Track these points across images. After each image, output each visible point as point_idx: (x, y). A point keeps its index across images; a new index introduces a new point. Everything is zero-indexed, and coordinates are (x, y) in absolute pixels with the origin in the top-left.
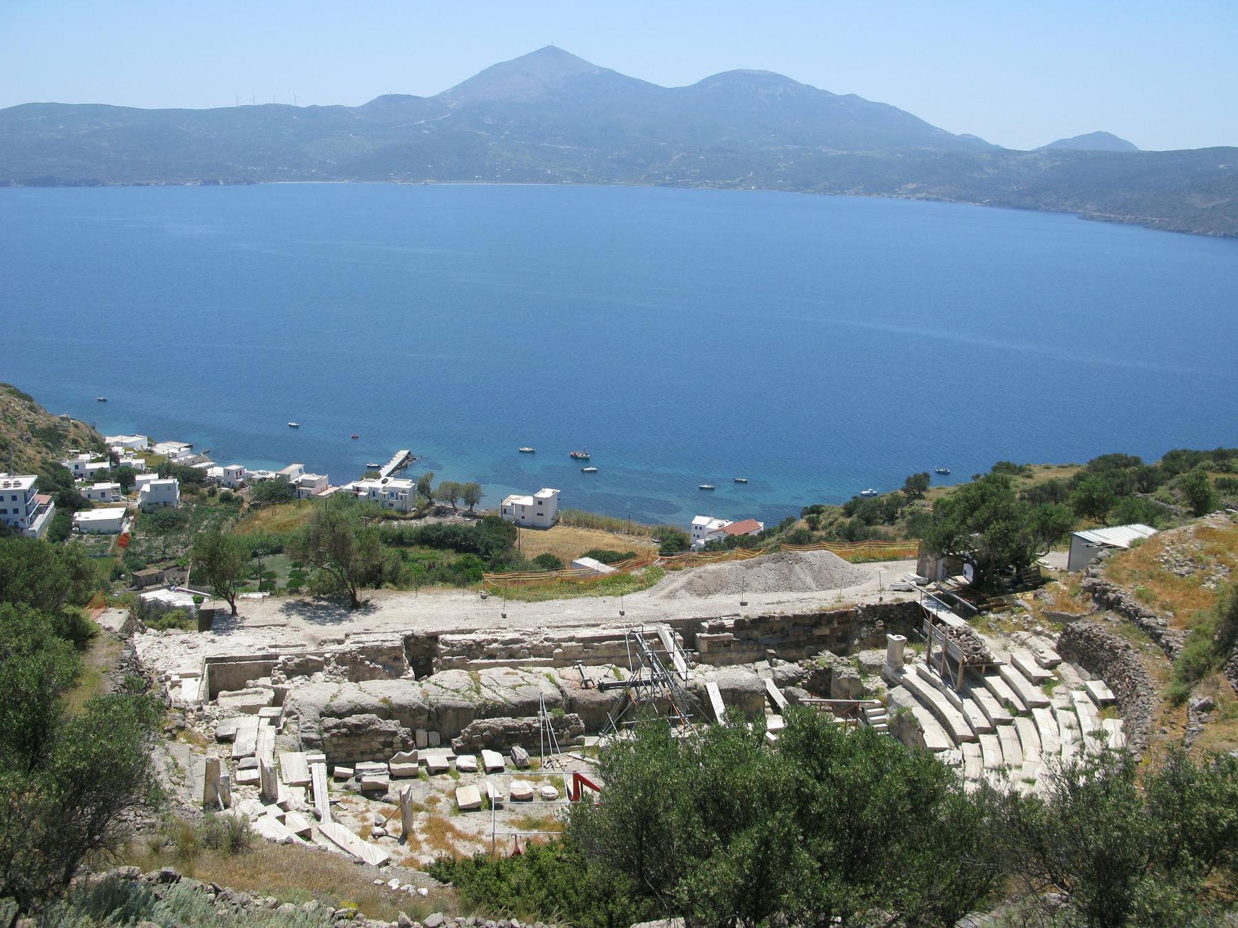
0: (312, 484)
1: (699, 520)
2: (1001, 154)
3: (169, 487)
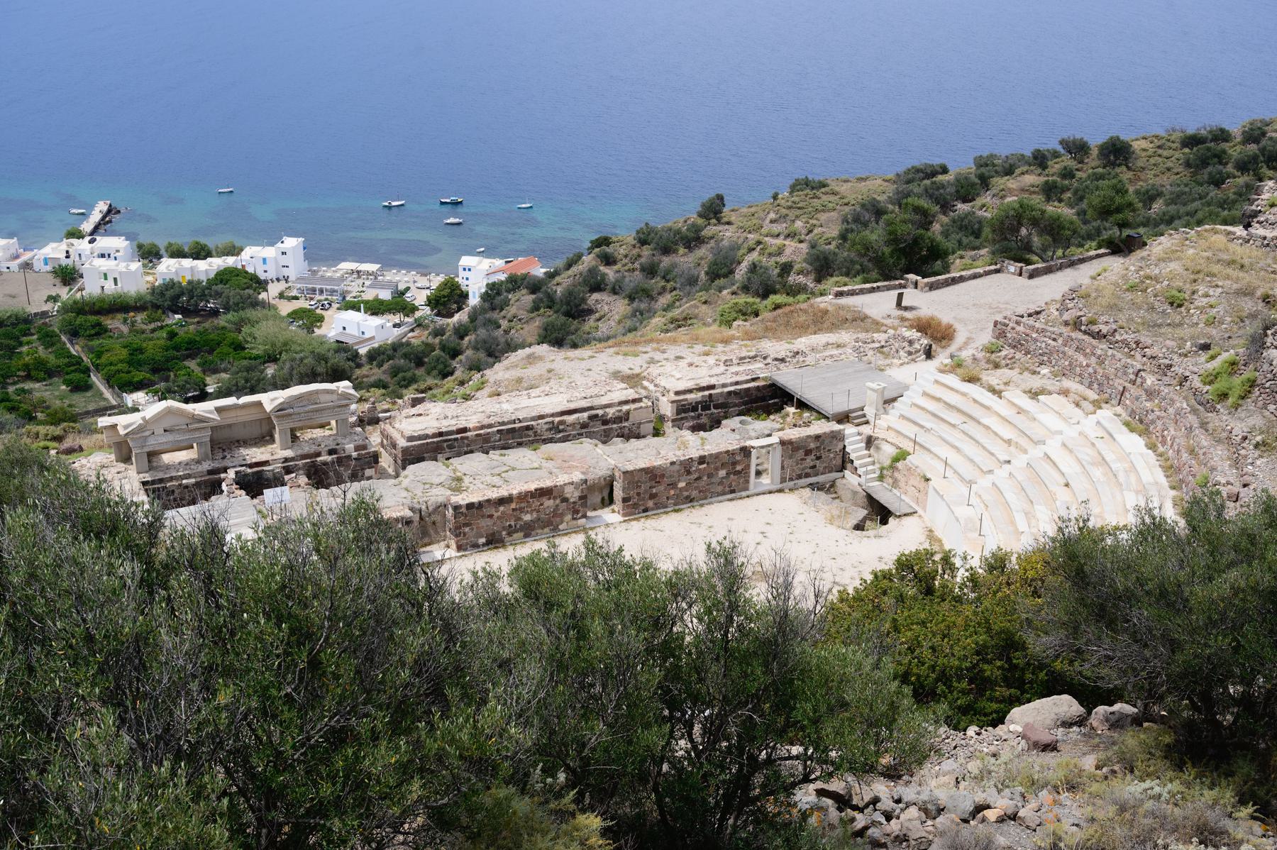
1: (466, 261)
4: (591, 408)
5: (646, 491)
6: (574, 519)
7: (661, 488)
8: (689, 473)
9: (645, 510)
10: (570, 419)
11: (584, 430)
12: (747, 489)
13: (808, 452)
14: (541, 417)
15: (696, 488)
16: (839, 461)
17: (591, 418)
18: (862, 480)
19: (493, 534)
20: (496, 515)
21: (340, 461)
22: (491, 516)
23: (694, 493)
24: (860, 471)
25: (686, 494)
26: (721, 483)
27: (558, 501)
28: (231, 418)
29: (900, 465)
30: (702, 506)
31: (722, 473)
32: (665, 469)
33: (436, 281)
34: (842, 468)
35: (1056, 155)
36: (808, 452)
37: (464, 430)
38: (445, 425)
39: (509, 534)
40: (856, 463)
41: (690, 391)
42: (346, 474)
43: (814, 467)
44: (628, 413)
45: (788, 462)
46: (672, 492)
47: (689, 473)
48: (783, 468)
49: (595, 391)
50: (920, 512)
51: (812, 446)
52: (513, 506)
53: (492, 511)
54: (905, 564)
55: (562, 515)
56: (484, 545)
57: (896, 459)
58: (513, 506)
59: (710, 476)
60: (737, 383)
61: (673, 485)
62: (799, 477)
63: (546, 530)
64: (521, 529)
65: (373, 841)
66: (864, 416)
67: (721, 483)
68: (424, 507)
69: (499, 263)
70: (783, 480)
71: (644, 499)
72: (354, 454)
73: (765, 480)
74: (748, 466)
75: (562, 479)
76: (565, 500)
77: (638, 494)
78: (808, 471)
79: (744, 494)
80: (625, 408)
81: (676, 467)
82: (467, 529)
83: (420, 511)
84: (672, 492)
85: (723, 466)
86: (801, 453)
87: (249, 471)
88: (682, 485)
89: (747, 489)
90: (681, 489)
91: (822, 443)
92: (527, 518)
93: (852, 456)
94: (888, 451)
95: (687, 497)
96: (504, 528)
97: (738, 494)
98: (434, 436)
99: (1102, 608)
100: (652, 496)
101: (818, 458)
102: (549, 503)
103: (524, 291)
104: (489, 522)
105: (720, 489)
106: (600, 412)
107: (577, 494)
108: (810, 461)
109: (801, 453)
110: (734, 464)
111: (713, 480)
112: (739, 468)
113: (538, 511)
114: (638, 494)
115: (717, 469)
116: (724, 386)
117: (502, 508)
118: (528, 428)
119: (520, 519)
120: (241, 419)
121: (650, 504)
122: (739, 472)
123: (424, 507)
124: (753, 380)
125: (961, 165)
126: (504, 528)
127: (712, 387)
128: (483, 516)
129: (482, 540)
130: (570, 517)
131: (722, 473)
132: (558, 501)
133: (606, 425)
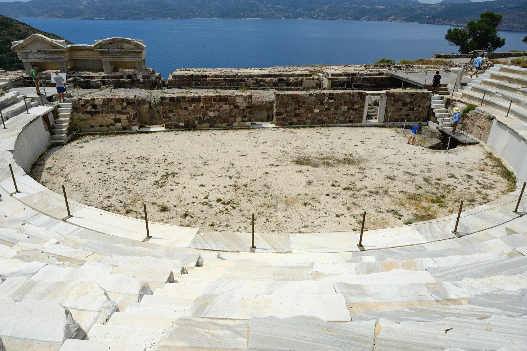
4: (281, 76)
5: (291, 111)
6: (243, 121)
7: (303, 110)
8: (322, 104)
9: (292, 124)
10: (267, 79)
12: (361, 122)
13: (405, 104)
15: (326, 115)
16: (425, 114)
18: (440, 126)
19: (189, 121)
20: (190, 108)
22: (186, 109)
23: (325, 119)
24: (439, 120)
25: (319, 118)
26: (343, 115)
27: (232, 107)
29: (469, 114)
30: (329, 126)
31: (345, 108)
32: (305, 98)
34: (427, 119)
36: (405, 104)
39: (200, 123)
40: (437, 115)
41: (341, 75)
43: (408, 115)
44: (302, 81)
45: (390, 109)
46: (310, 115)
47: (322, 104)
48: (386, 112)
50: (482, 143)
51: (408, 100)
52: (201, 104)
53: (187, 105)
54: (404, 268)
55: (235, 117)
56: (183, 127)
57: (467, 111)
58: (201, 104)
59: (336, 108)
60: (370, 75)
61: (311, 110)
62: (397, 120)
63: (225, 125)
64: (208, 121)
66: (446, 89)
67: (343, 115)
68: (153, 101)
70: (385, 120)
71: (290, 116)
72: (141, 80)
73: (374, 121)
74: (363, 107)
76: (237, 107)
77: (287, 112)
78: (404, 117)
79: (358, 124)
80: (300, 78)
81: (313, 98)
82: (171, 115)
83: (150, 103)
84: (310, 115)
85: (346, 103)
86: (400, 104)
87: (82, 80)
88: (317, 111)
89: (361, 122)
90: (316, 114)
91: (415, 100)
92: (211, 114)
93: (435, 110)
94: (459, 108)
95: (320, 120)
96: (196, 119)
97: (354, 124)
100: (296, 115)
101: (412, 110)
102: (226, 107)
104: (185, 113)
105: (342, 118)
106: (285, 78)
107: (245, 104)
108: (405, 111)
109: (400, 104)
110: (354, 103)
111: (338, 112)
112: (356, 106)
113: (219, 111)
114: (287, 112)
115: (341, 105)
116: (362, 75)
117: (193, 105)
119: (206, 114)
120: (91, 57)
121: (295, 120)
122: (356, 110)
123: (153, 101)
124: (380, 74)
126: (196, 119)
128: (181, 108)
129: (182, 124)
130: (239, 119)
131: (345, 108)
132: (232, 107)
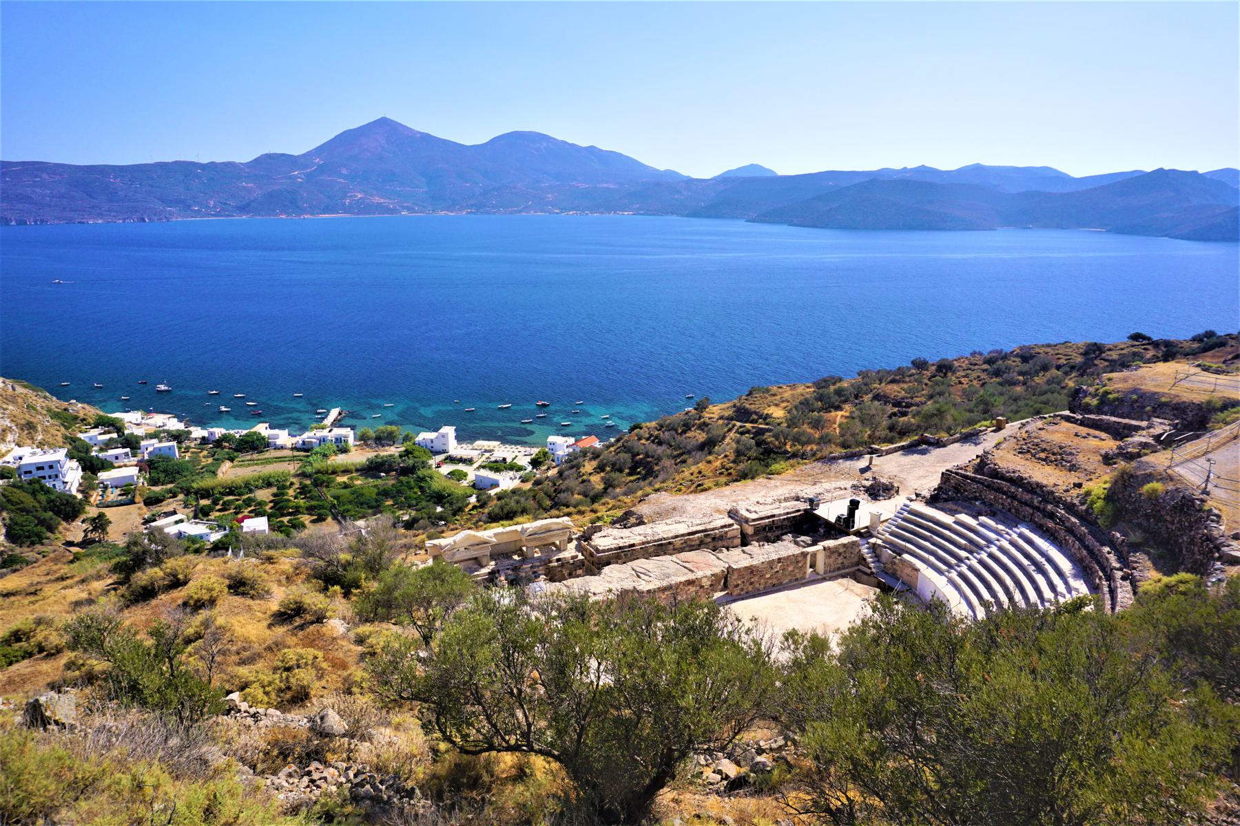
0: (276, 437)
1: (551, 439)
2: (690, 181)
3: (170, 448)
11: (700, 545)
13: (840, 554)
14: (677, 537)
17: (706, 536)
21: (562, 565)
28: (505, 539)
33: (535, 451)
35: (909, 369)
37: (633, 545)
38: (621, 543)
42: (566, 573)
49: (706, 520)
65: (931, 718)
69: (571, 440)
75: (699, 574)
76: (702, 587)
98: (616, 549)
99: (475, 783)
102: (692, 589)
103: (126, 432)
118: (670, 543)
125: (1115, 336)
127: (773, 516)
133: (712, 541)
